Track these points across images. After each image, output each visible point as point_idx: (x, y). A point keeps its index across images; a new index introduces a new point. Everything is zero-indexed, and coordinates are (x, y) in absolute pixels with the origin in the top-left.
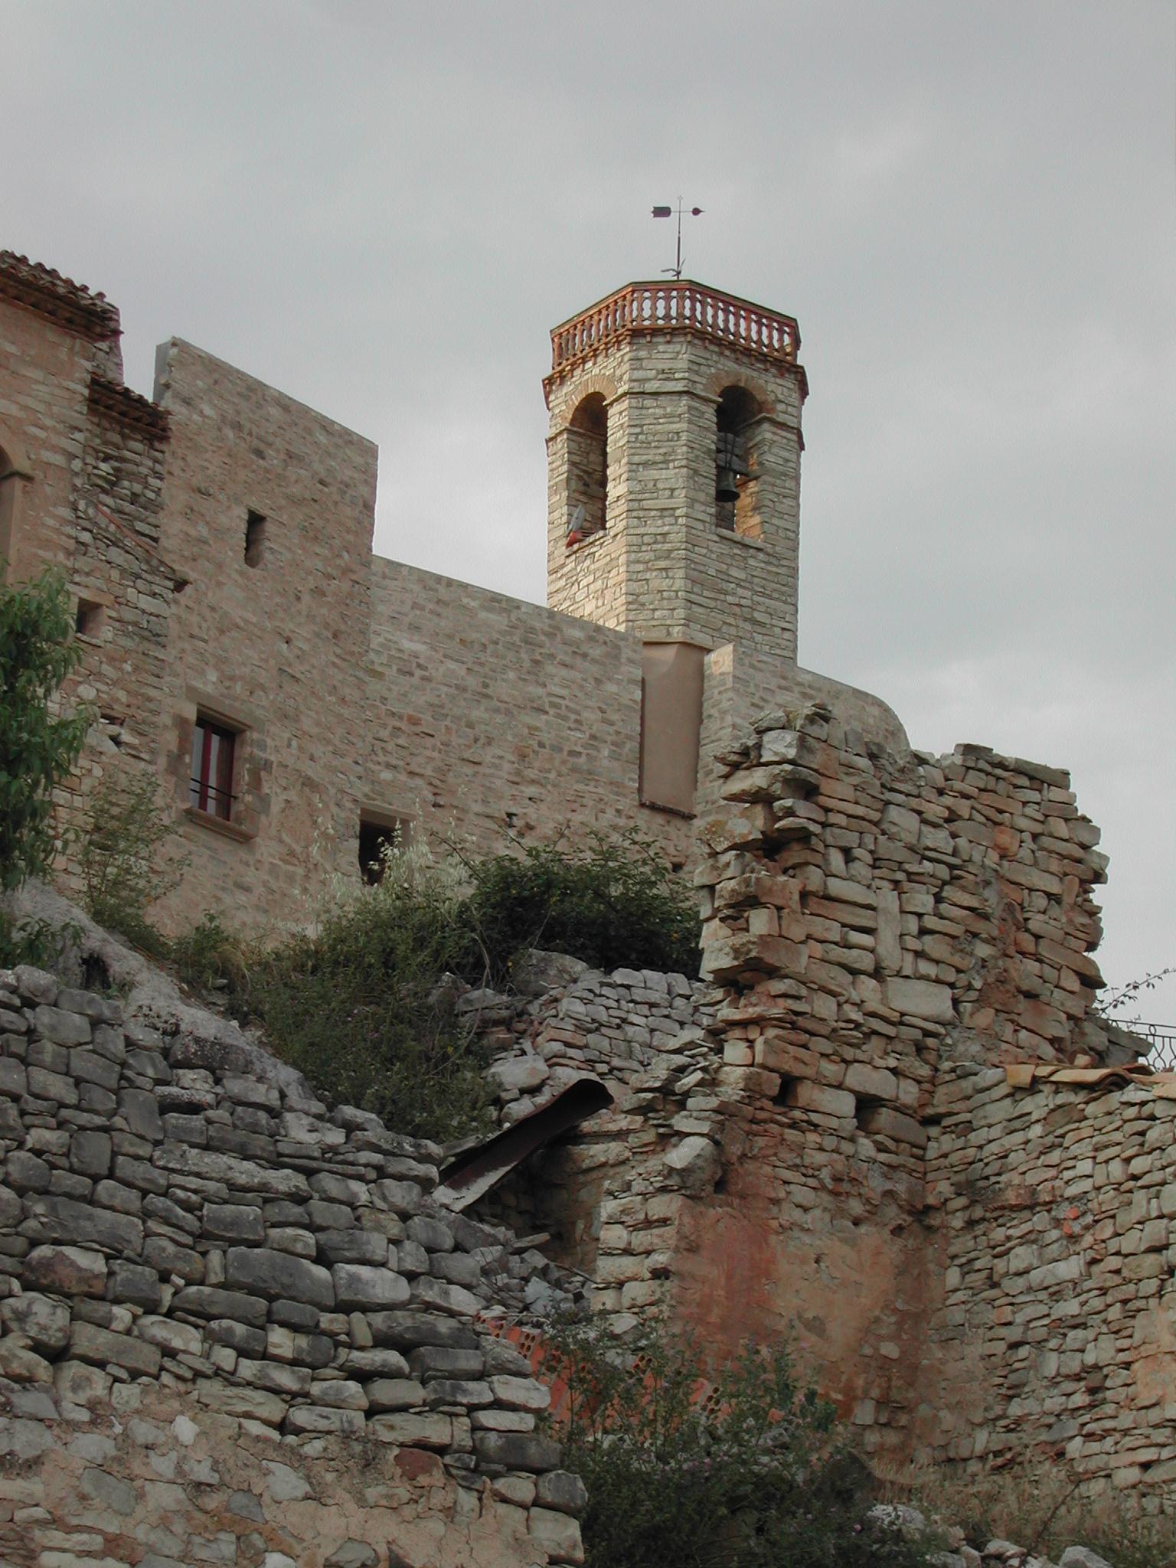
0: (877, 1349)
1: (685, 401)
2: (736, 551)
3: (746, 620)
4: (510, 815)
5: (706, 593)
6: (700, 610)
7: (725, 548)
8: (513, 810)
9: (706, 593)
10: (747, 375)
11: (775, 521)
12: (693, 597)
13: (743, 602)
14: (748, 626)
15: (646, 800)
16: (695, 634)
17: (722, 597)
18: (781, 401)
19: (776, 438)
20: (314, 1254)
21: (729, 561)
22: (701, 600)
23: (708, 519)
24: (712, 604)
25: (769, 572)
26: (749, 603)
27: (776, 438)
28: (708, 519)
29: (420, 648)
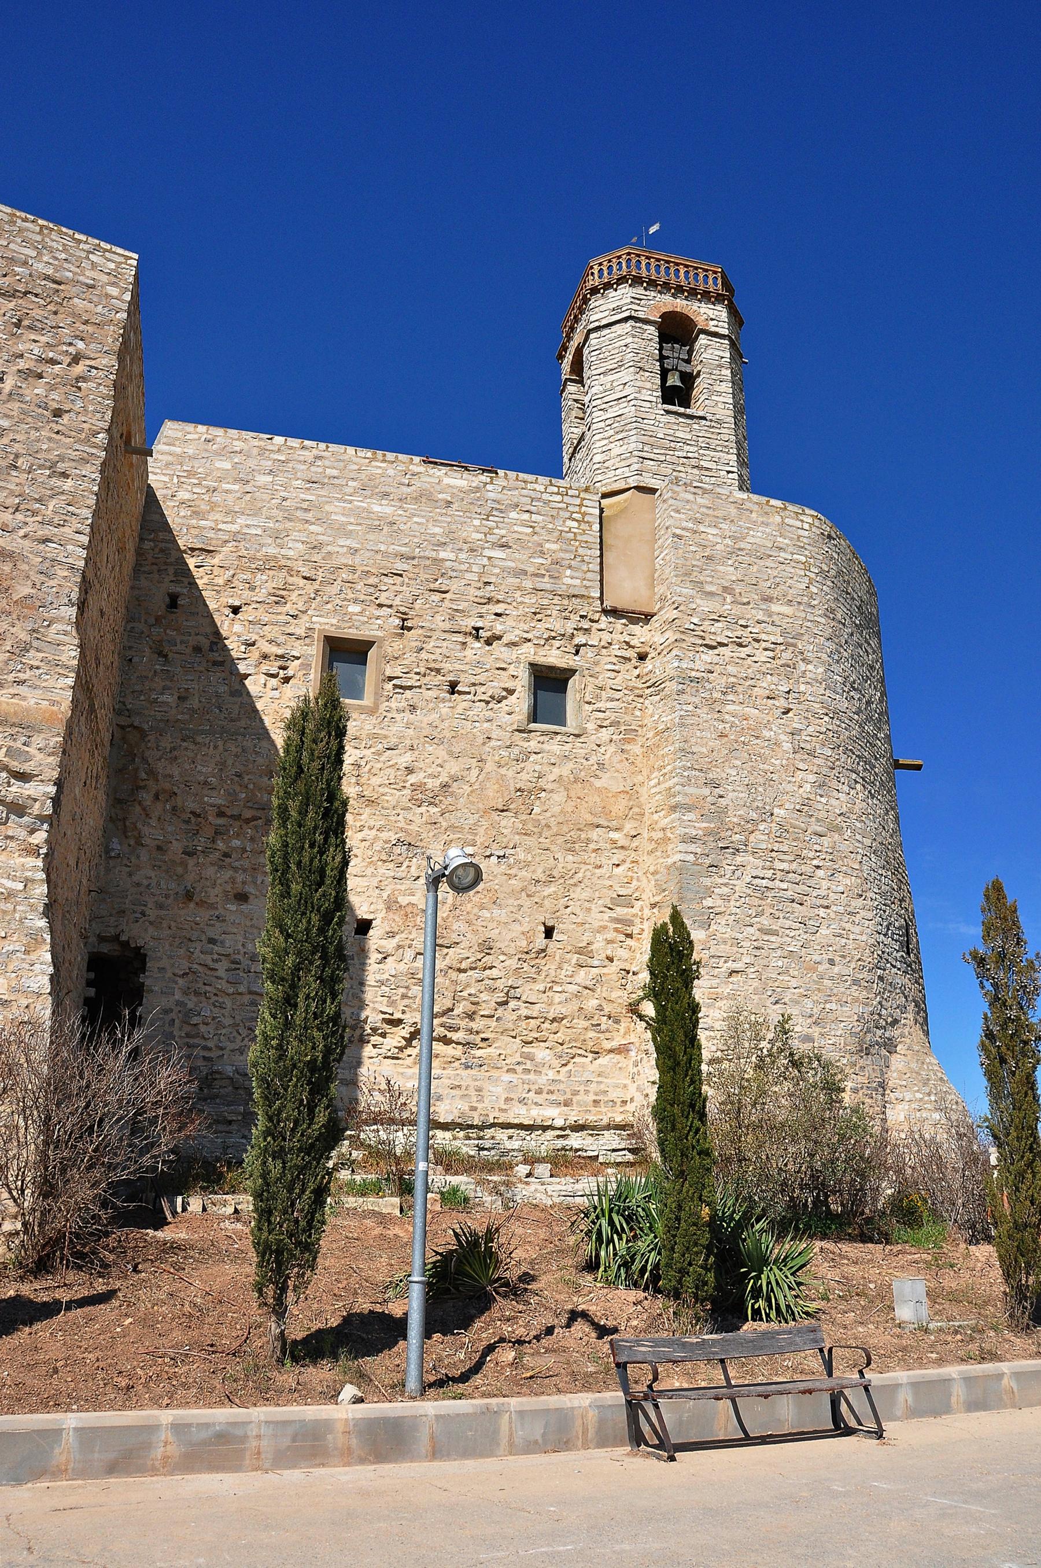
0: (995, 1167)
1: (631, 323)
2: (681, 420)
3: (694, 467)
4: (477, 629)
5: (655, 451)
6: (652, 463)
7: (672, 419)
8: (479, 624)
9: (655, 451)
10: (680, 304)
11: (714, 398)
12: (644, 454)
13: (690, 455)
14: (696, 471)
15: (608, 604)
16: (647, 480)
17: (671, 453)
18: (712, 319)
19: (709, 343)
20: (247, 682)
21: (676, 427)
22: (652, 456)
23: (654, 399)
24: (663, 458)
25: (713, 433)
26: (696, 455)
27: (709, 343)
28: (654, 399)
29: (389, 510)
